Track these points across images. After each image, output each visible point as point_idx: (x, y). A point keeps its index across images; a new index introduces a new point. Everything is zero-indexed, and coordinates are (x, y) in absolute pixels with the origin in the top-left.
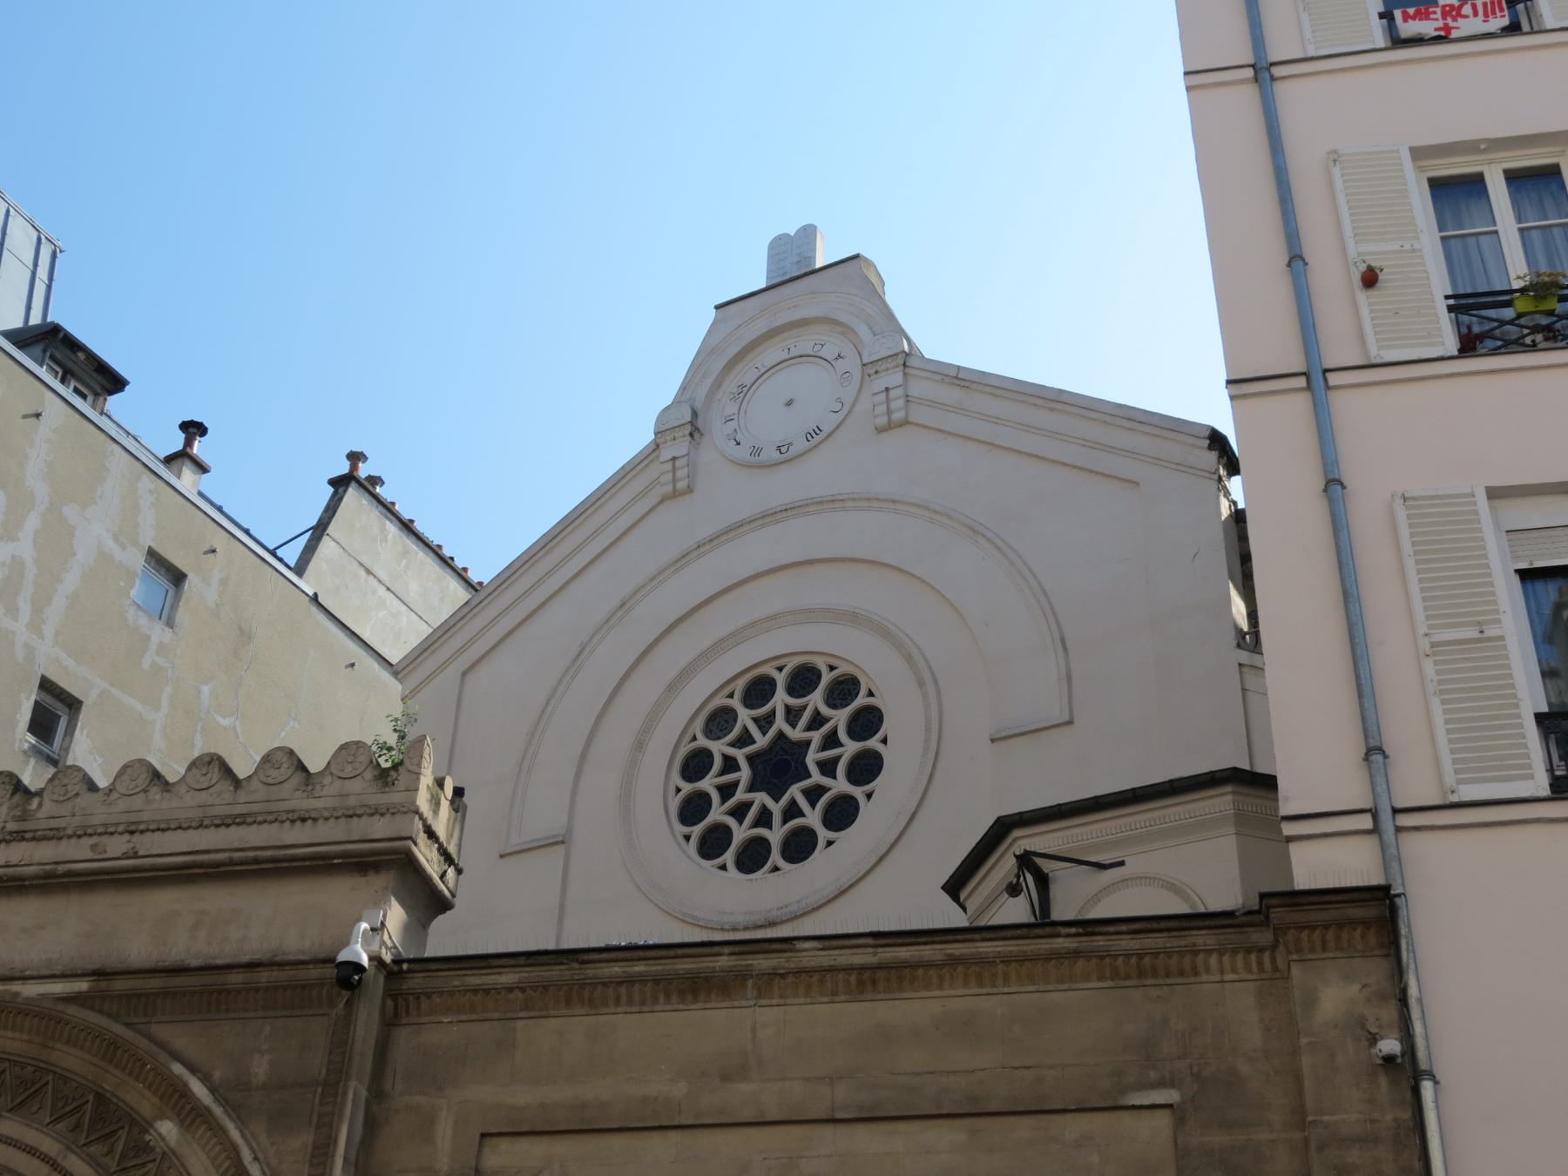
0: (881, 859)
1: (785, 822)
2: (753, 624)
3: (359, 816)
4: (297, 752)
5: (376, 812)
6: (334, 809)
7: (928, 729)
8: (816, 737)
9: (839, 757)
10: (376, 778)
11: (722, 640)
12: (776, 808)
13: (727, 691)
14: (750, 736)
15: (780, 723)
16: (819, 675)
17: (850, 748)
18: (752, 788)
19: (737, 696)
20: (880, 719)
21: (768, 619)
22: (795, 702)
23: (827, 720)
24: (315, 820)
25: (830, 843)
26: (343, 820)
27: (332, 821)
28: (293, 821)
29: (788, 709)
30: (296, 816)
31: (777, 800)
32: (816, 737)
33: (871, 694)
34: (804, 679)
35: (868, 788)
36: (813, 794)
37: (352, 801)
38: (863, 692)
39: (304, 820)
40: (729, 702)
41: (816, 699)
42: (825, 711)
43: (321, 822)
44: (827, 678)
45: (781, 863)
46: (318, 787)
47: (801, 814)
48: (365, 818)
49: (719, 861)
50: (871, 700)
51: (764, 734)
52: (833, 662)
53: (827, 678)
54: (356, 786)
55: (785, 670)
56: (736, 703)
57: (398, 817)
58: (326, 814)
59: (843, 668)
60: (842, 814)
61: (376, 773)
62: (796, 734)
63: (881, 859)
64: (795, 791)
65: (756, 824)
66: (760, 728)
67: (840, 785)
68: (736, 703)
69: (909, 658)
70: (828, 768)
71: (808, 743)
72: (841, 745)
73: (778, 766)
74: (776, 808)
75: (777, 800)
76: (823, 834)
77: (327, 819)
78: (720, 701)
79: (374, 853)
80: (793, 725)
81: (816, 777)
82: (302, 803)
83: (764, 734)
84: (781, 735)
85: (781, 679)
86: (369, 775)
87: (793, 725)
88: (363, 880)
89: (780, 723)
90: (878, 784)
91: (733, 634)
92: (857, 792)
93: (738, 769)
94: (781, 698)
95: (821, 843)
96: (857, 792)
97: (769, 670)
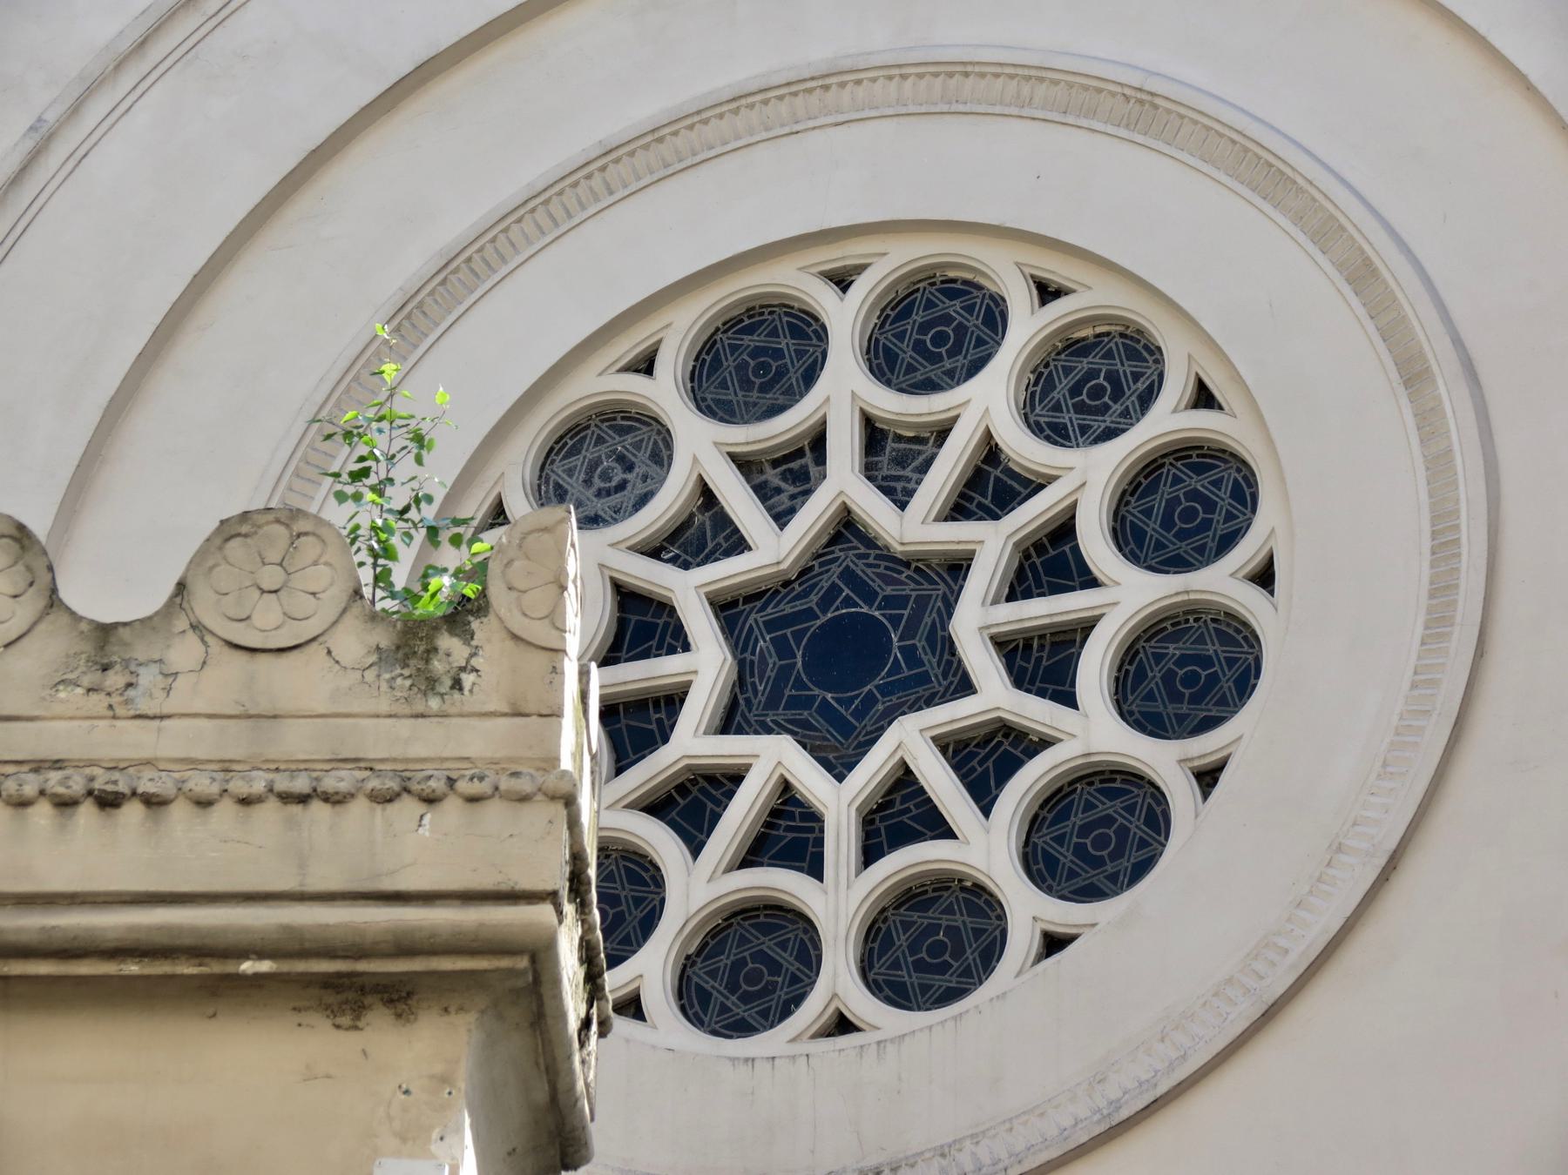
0: (1271, 1014)
1: (870, 855)
2: (737, 101)
3: (335, 799)
4: (206, 535)
5: (406, 788)
6: (226, 767)
7: (1444, 546)
8: (993, 544)
9: (1086, 627)
10: (383, 657)
11: (610, 153)
12: (839, 802)
13: (629, 346)
14: (723, 522)
15: (844, 481)
16: (995, 317)
17: (1126, 594)
18: (730, 721)
19: (672, 365)
20: (1245, 494)
21: (794, 87)
22: (891, 404)
23: (1034, 486)
24: (153, 802)
25: (1053, 943)
26: (270, 811)
27: (225, 811)
28: (65, 804)
29: (874, 434)
30: (77, 786)
31: (839, 769)
32: (993, 544)
33: (1204, 398)
34: (935, 327)
35: (1204, 746)
36: (986, 758)
37: (297, 741)
38: (1175, 388)
39: (108, 802)
40: (635, 387)
41: (987, 404)
42: (1025, 449)
43: (179, 812)
44: (1027, 327)
45: (862, 1004)
46: (147, 677)
47: (938, 826)
48: (359, 808)
49: (812, 1009)
50: (1203, 423)
51: (782, 518)
52: (1057, 269)
53: (1027, 327)
54: (301, 683)
55: (862, 288)
56: (664, 393)
57: (494, 811)
58: (202, 784)
59: (1093, 297)
60: (1100, 837)
61: (383, 637)
62: (911, 527)
63: (1271, 1014)
64: (911, 741)
65: (755, 853)
66: (763, 492)
67: (1090, 729)
68: (664, 393)
69: (1362, 275)
70: (1043, 663)
71: (958, 567)
72: (1091, 582)
73: (841, 644)
74: (839, 802)
75: (839, 769)
76: (1027, 909)
77: (204, 803)
78: (601, 383)
79: (405, 946)
80: (900, 498)
81: (994, 695)
82: (82, 734)
83: (782, 518)
84: (846, 528)
85: (845, 319)
86: (354, 642)
87: (900, 498)
88: (348, 1043)
89: (844, 481)
90: (1241, 735)
91: (655, 135)
92: (1163, 760)
93: (677, 640)
94: (844, 391)
95: (1021, 939)
96: (1163, 760)
97: (798, 281)
